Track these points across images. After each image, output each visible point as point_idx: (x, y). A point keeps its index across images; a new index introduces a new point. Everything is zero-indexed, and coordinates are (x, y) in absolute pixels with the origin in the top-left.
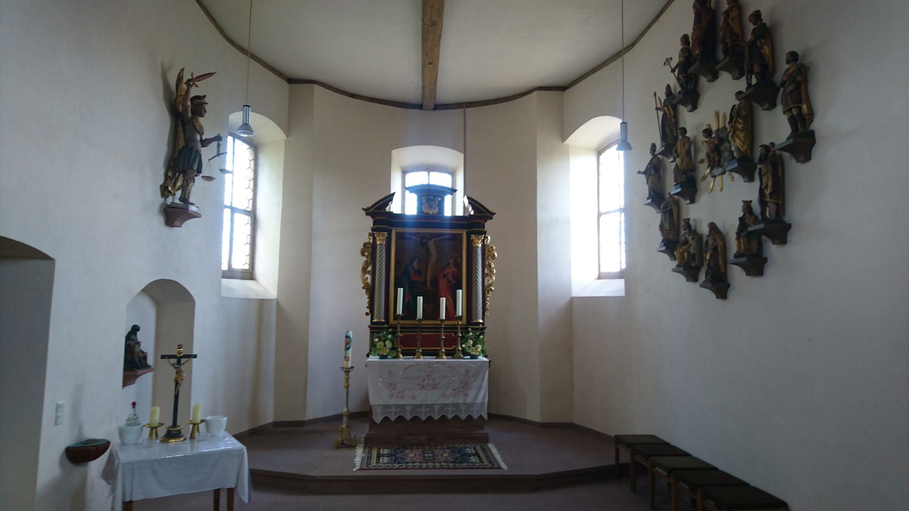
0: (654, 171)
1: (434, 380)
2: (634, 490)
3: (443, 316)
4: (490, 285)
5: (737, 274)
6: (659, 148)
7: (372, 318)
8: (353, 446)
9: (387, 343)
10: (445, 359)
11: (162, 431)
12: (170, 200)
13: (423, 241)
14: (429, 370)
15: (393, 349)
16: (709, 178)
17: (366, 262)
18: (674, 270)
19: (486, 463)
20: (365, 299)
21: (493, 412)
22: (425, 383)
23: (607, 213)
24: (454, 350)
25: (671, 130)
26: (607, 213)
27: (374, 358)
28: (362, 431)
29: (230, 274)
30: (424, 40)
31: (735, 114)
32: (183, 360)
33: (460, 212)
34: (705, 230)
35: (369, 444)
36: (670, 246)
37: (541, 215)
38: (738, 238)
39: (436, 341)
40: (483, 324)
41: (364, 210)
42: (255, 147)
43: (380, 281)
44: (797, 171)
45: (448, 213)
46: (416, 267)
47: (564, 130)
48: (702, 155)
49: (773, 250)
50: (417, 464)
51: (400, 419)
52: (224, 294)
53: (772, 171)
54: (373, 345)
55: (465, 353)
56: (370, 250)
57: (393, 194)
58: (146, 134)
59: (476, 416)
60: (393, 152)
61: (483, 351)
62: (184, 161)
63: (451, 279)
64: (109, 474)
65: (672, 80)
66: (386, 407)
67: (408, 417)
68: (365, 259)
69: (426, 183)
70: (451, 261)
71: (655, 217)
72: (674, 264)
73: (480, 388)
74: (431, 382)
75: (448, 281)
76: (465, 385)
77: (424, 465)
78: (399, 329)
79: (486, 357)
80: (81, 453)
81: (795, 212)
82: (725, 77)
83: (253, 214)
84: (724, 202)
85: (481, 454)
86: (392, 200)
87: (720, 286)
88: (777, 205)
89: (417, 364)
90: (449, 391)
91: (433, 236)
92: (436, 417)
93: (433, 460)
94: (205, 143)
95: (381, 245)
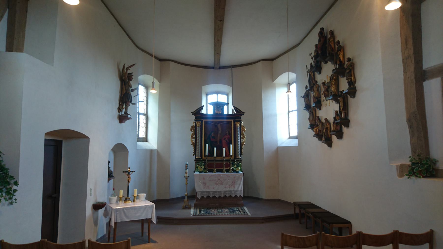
0: (307, 96)
2: (301, 223)
3: (224, 155)
4: (243, 142)
5: (334, 138)
6: (308, 88)
7: (196, 157)
8: (190, 208)
10: (225, 173)
11: (124, 199)
12: (120, 114)
13: (215, 124)
15: (204, 169)
16: (325, 101)
17: (193, 134)
18: (314, 136)
19: (242, 213)
21: (246, 195)
23: (292, 111)
24: (229, 169)
25: (312, 81)
26: (292, 111)
27: (197, 173)
28: (193, 203)
29: (139, 140)
31: (332, 78)
32: (130, 173)
33: (230, 113)
34: (324, 121)
35: (196, 207)
36: (312, 126)
37: (264, 112)
38: (333, 125)
39: (221, 166)
40: (241, 158)
42: (147, 88)
43: (199, 141)
44: (351, 100)
45: (225, 112)
47: (273, 77)
48: (322, 93)
49: (345, 129)
50: (215, 214)
51: (208, 197)
52: (138, 148)
53: (343, 100)
54: (196, 168)
55: (234, 170)
56: (194, 129)
57: (203, 106)
58: (112, 89)
59: (238, 196)
60: (203, 87)
61: (241, 169)
62: (126, 98)
64: (106, 214)
65: (312, 61)
66: (202, 192)
67: (211, 196)
68: (192, 132)
69: (216, 101)
70: (227, 133)
71: (307, 114)
72: (314, 133)
73: (240, 184)
74: (220, 182)
76: (234, 183)
77: (218, 214)
79: (242, 172)
80: (97, 207)
81: (352, 116)
82: (329, 63)
83: (146, 115)
84: (329, 110)
85: (241, 210)
87: (329, 143)
88: (345, 113)
89: (214, 175)
90: (227, 186)
92: (222, 196)
93: (222, 212)
94: (132, 90)
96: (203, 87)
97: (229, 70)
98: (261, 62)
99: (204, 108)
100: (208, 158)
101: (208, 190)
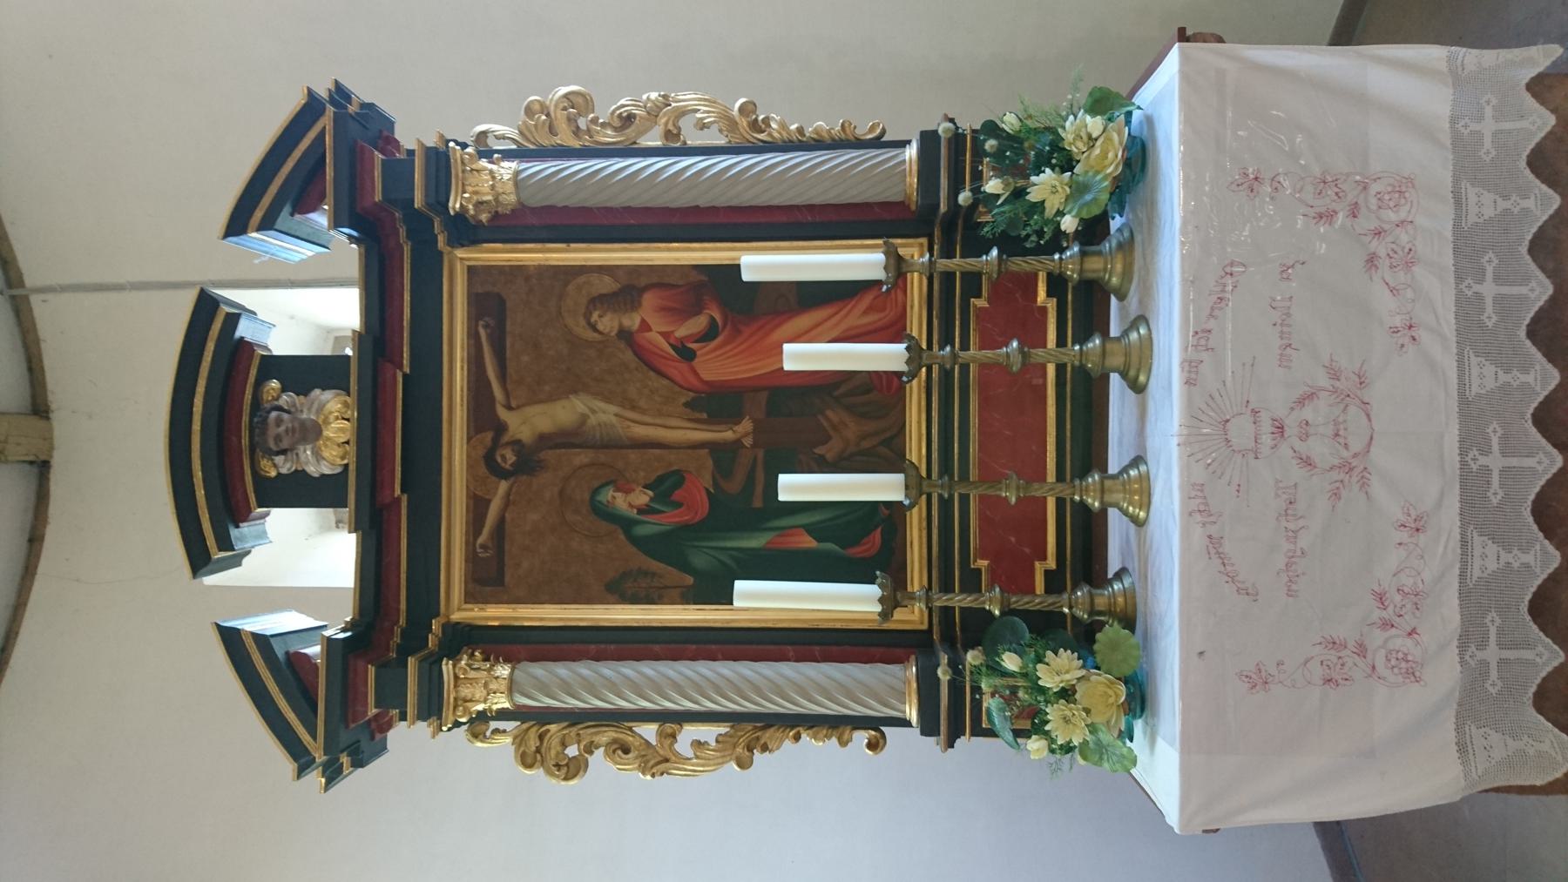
3: (885, 356)
4: (732, 124)
9: (1049, 680)
14: (1241, 431)
15: (1083, 638)
22: (1319, 449)
46: (642, 498)
59: (1539, 121)
61: (1102, 103)
63: (698, 324)
66: (1472, 706)
68: (598, 759)
70: (608, 323)
76: (1340, 196)
78: (959, 600)
90: (1384, 302)
95: (512, 687)
97: (43, 311)
100: (916, 578)
101: (1447, 614)
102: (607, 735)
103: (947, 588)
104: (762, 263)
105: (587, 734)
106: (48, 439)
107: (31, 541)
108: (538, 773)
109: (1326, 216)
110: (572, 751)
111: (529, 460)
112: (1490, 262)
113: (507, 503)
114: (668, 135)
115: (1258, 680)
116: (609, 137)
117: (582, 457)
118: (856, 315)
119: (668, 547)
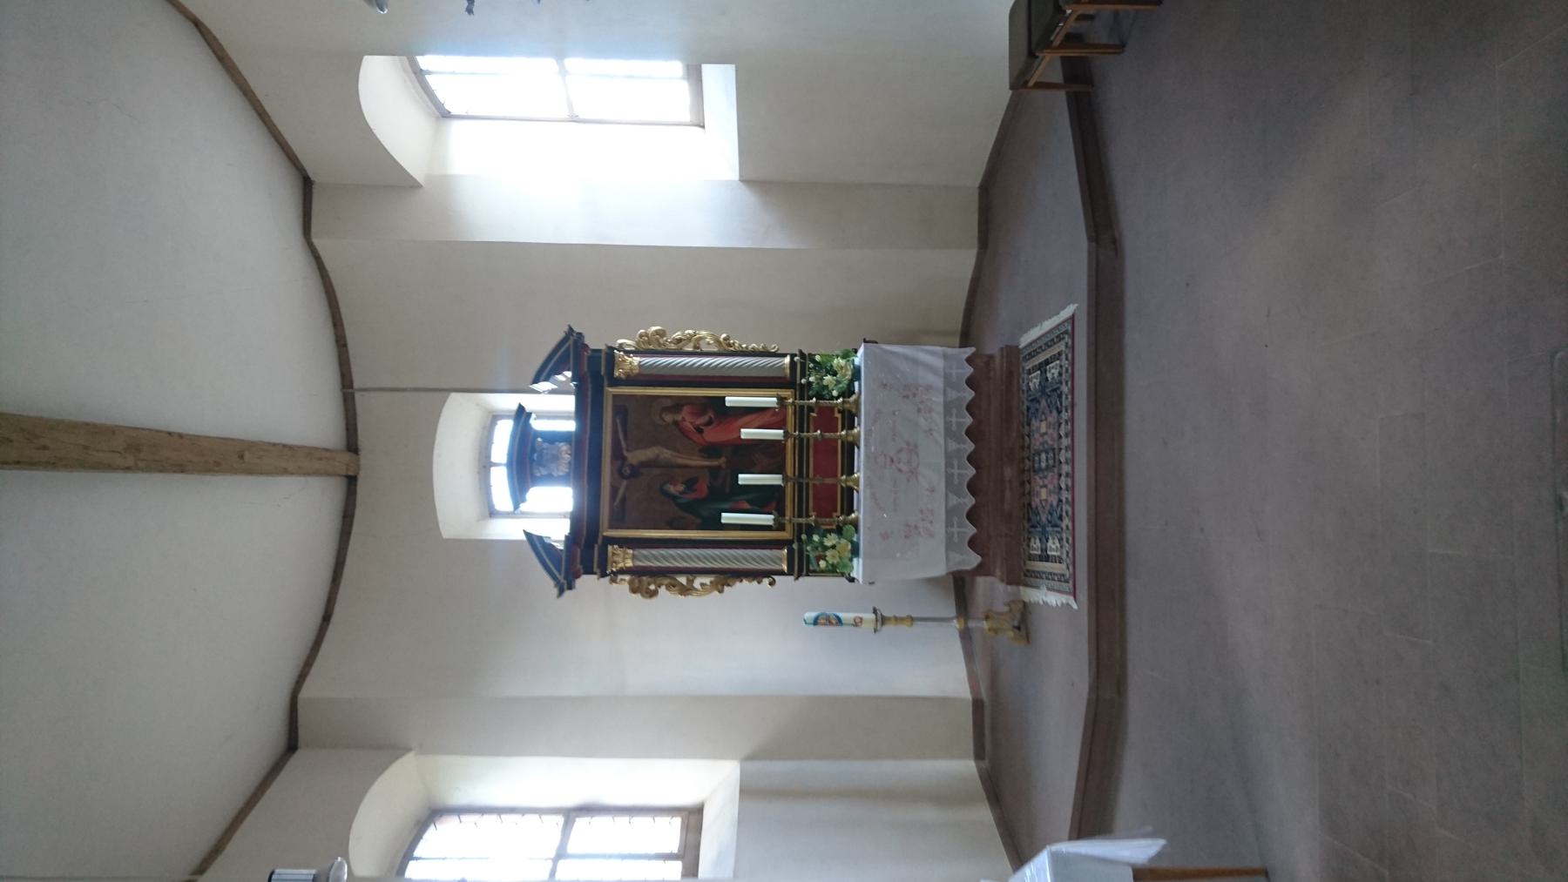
1: (900, 451)
3: (776, 434)
15: (839, 531)
20: (745, 587)
30: (181, 468)
41: (561, 592)
42: (434, 813)
46: (681, 488)
57: (528, 534)
59: (969, 370)
61: (845, 356)
63: (705, 419)
68: (662, 590)
70: (668, 418)
74: (904, 456)
75: (709, 423)
76: (910, 391)
86: (540, 538)
90: (921, 420)
91: (618, 455)
95: (634, 557)
96: (445, 536)
97: (359, 399)
98: (315, 241)
99: (540, 528)
101: (942, 514)
102: (667, 581)
103: (800, 516)
104: (734, 399)
105: (659, 580)
106: (358, 466)
107: (345, 517)
108: (638, 596)
109: (906, 397)
110: (652, 587)
111: (636, 471)
112: (954, 411)
113: (627, 488)
114: (696, 347)
115: (885, 536)
116: (673, 347)
117: (657, 471)
118: (767, 418)
119: (690, 507)
